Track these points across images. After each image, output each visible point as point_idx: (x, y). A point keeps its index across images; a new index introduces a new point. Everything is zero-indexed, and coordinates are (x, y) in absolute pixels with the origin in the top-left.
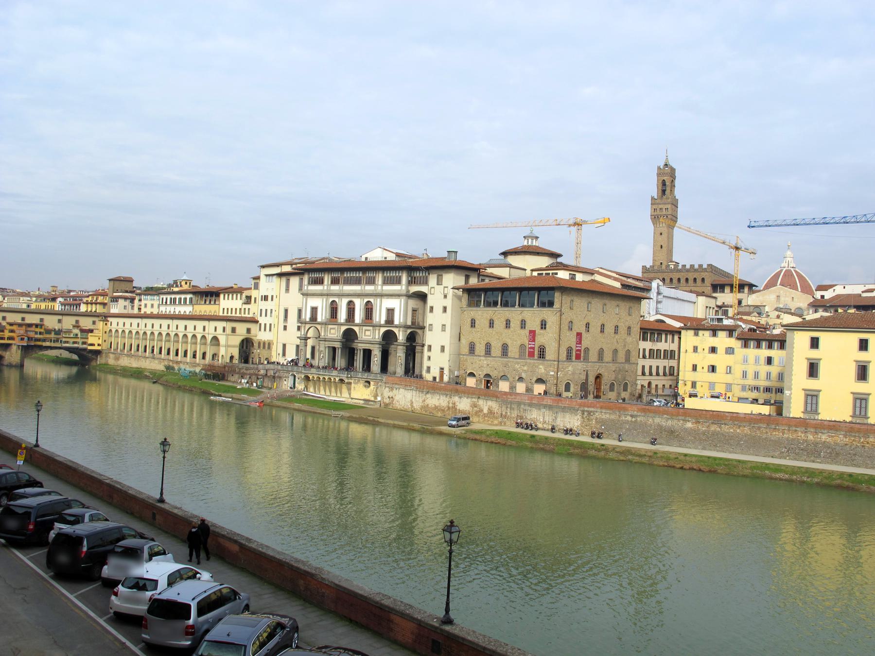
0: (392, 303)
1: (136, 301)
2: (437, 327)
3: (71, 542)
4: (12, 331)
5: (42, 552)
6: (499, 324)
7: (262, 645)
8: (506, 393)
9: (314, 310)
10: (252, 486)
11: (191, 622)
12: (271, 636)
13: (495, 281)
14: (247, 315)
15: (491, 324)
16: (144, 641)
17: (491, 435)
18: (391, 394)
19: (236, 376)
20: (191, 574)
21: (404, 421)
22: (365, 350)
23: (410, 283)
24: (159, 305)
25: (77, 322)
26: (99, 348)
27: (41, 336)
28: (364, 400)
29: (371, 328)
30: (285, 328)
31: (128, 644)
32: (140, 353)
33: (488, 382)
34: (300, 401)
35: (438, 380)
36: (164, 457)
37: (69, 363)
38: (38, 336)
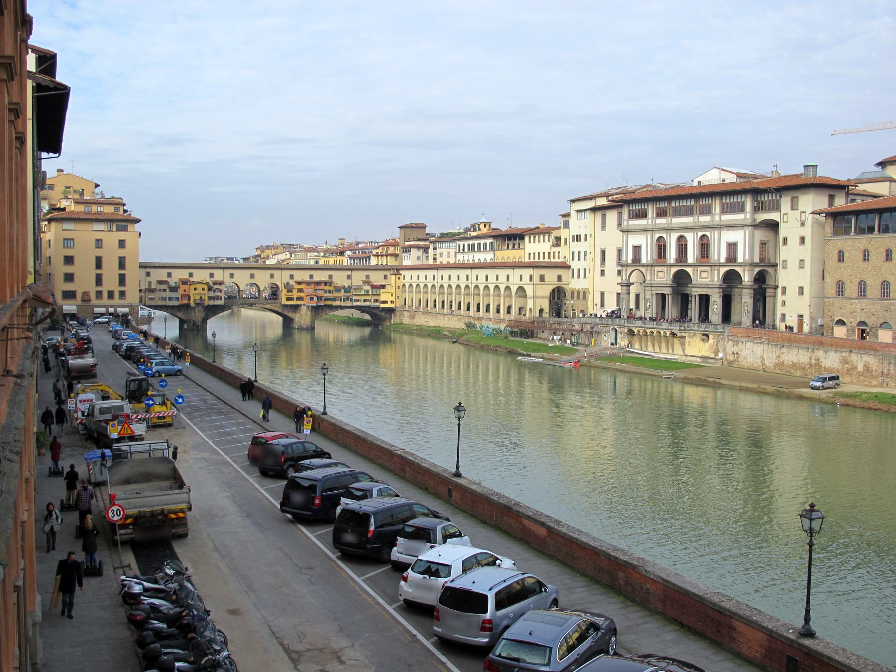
0: (734, 237)
1: (431, 251)
2: (793, 264)
3: (359, 519)
4: (300, 291)
5: (328, 530)
6: (877, 256)
7: (571, 649)
8: (887, 345)
9: (637, 249)
10: (567, 464)
11: (488, 616)
12: (582, 639)
13: (870, 200)
14: (556, 260)
15: (866, 256)
16: (436, 634)
17: (868, 399)
18: (735, 349)
19: (547, 332)
20: (491, 559)
21: (754, 382)
22: (701, 296)
23: (756, 209)
24: (456, 253)
25: (367, 277)
26: (392, 305)
27: (330, 295)
28: (702, 357)
29: (708, 268)
30: (603, 273)
31: (420, 636)
32: (437, 310)
33: (863, 331)
34: (624, 360)
35: (795, 330)
36: (459, 425)
37: (362, 323)
38: (327, 295)
